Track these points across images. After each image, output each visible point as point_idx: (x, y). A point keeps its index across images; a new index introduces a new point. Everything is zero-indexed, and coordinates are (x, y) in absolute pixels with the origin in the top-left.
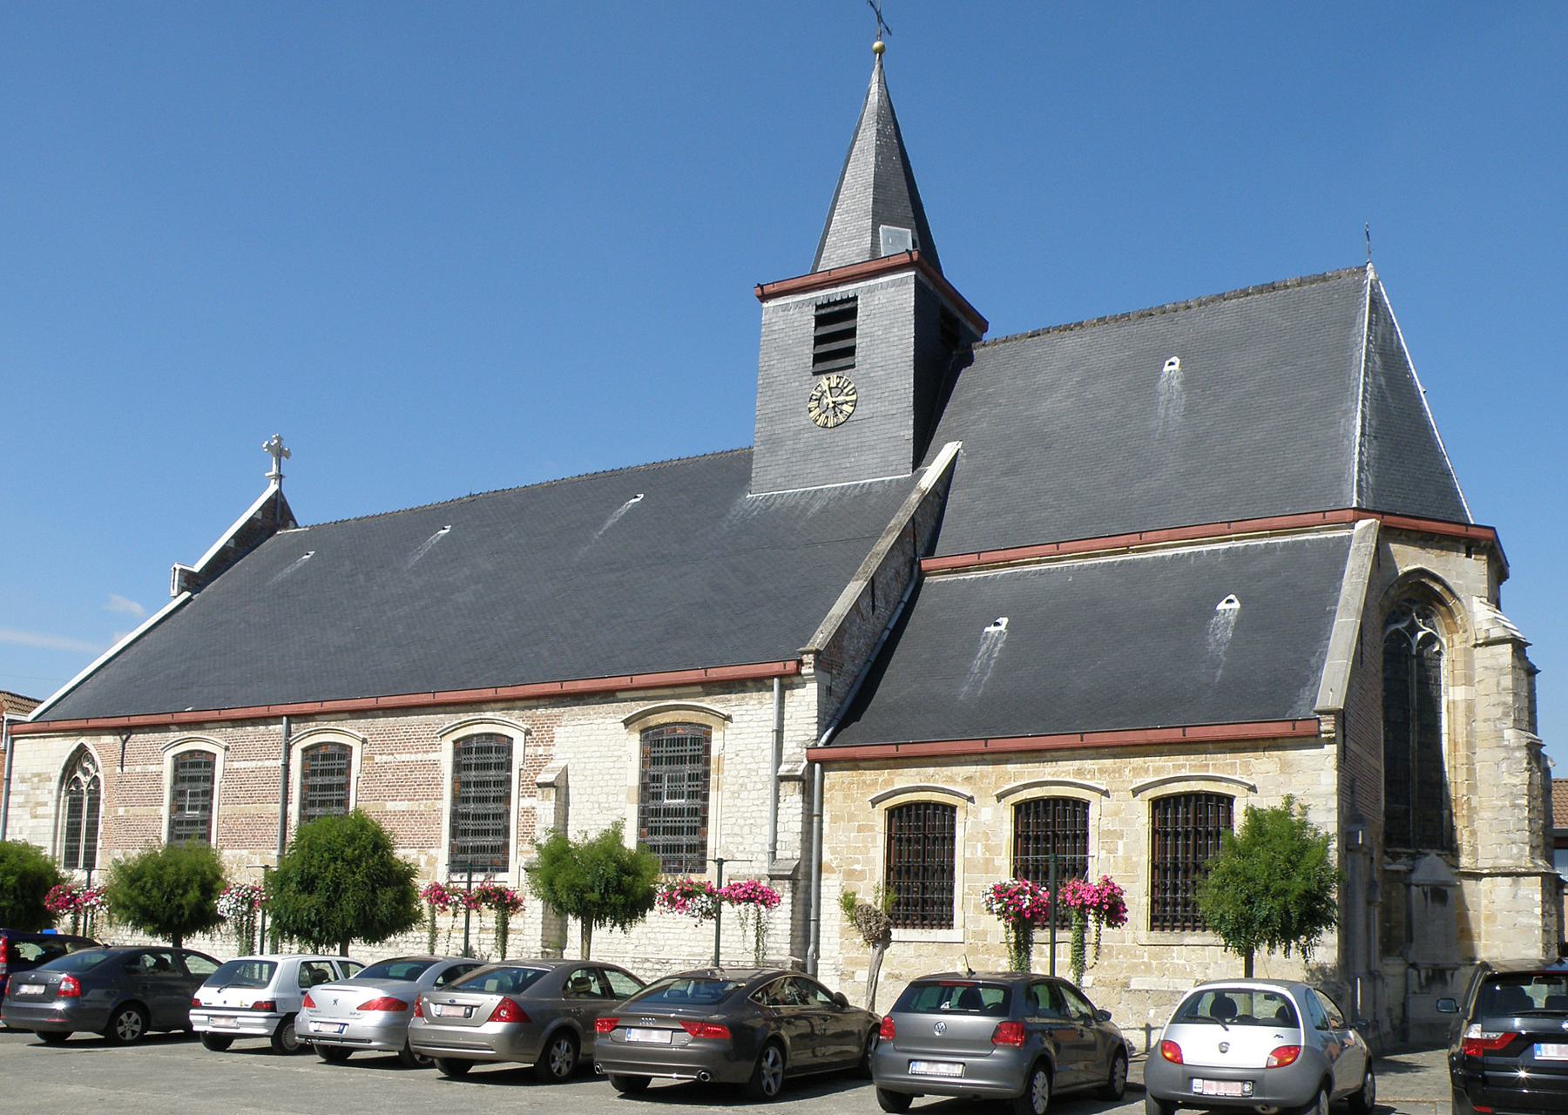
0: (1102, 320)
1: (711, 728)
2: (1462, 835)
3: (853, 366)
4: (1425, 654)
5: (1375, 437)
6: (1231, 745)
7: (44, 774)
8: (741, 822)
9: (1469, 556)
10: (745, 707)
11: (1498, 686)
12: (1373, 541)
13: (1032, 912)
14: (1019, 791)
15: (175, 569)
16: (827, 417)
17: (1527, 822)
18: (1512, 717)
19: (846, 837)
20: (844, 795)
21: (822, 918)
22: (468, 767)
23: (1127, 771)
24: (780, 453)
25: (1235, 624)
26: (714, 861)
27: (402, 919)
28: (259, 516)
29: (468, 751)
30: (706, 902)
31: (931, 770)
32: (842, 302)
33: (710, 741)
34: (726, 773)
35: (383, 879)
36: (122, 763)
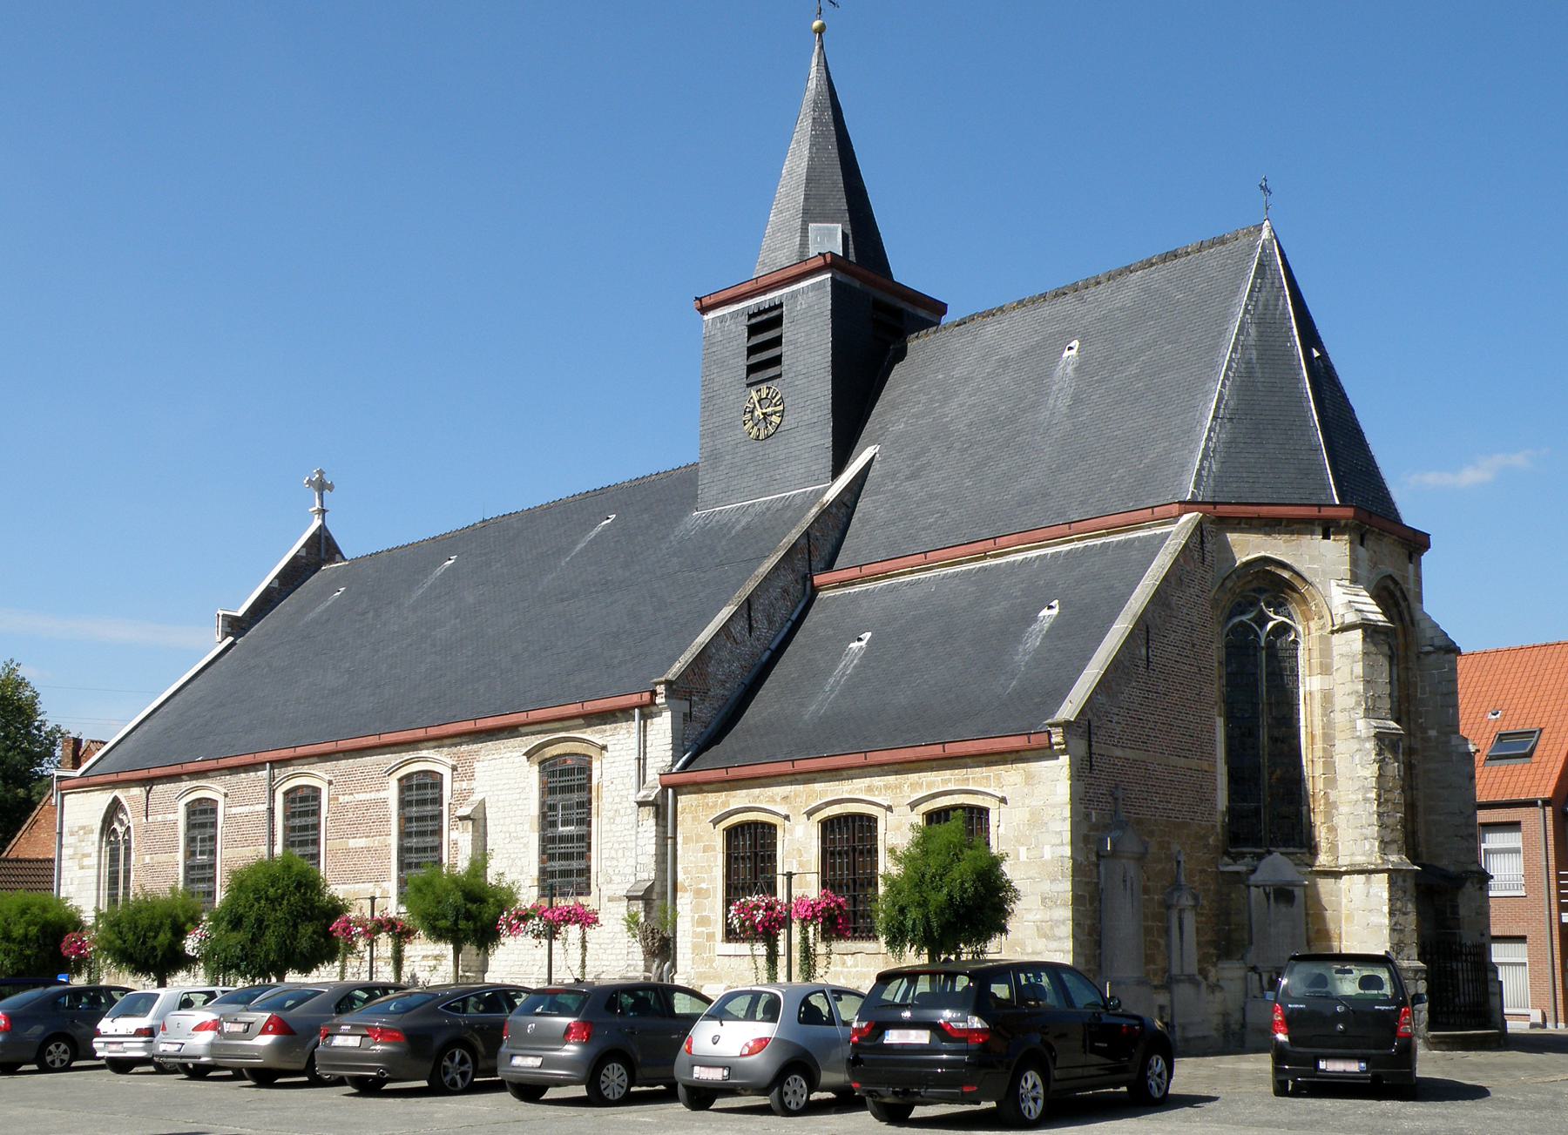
0: (1021, 303)
1: (591, 757)
2: (1320, 832)
3: (780, 376)
4: (1278, 645)
5: (1231, 419)
6: (983, 759)
7: (88, 826)
8: (616, 846)
11: (1352, 674)
12: (1184, 537)
13: (763, 926)
14: (823, 809)
15: (218, 615)
16: (759, 429)
17: (1376, 816)
18: (1364, 706)
19: (695, 857)
20: (693, 817)
21: (678, 935)
22: (410, 803)
23: (906, 786)
24: (721, 468)
25: (1047, 632)
26: (783, 875)
27: (326, 949)
28: (303, 553)
29: (410, 788)
30: (538, 925)
31: (757, 791)
32: (771, 309)
33: (591, 770)
34: (604, 800)
35: (305, 914)
36: (147, 813)
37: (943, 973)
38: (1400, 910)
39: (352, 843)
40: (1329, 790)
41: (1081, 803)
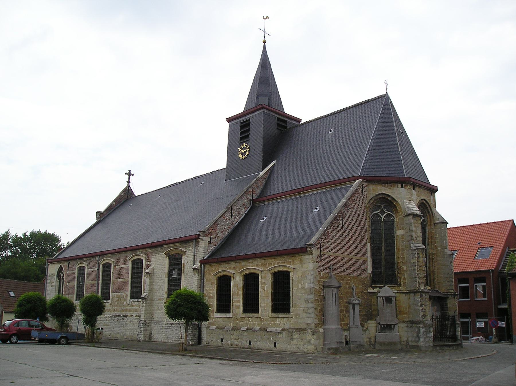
3: (249, 140)
9: (402, 187)
10: (189, 249)
23: (267, 264)
34: (185, 268)
38: (424, 305)
39: (119, 280)
40: (404, 267)
41: (317, 270)
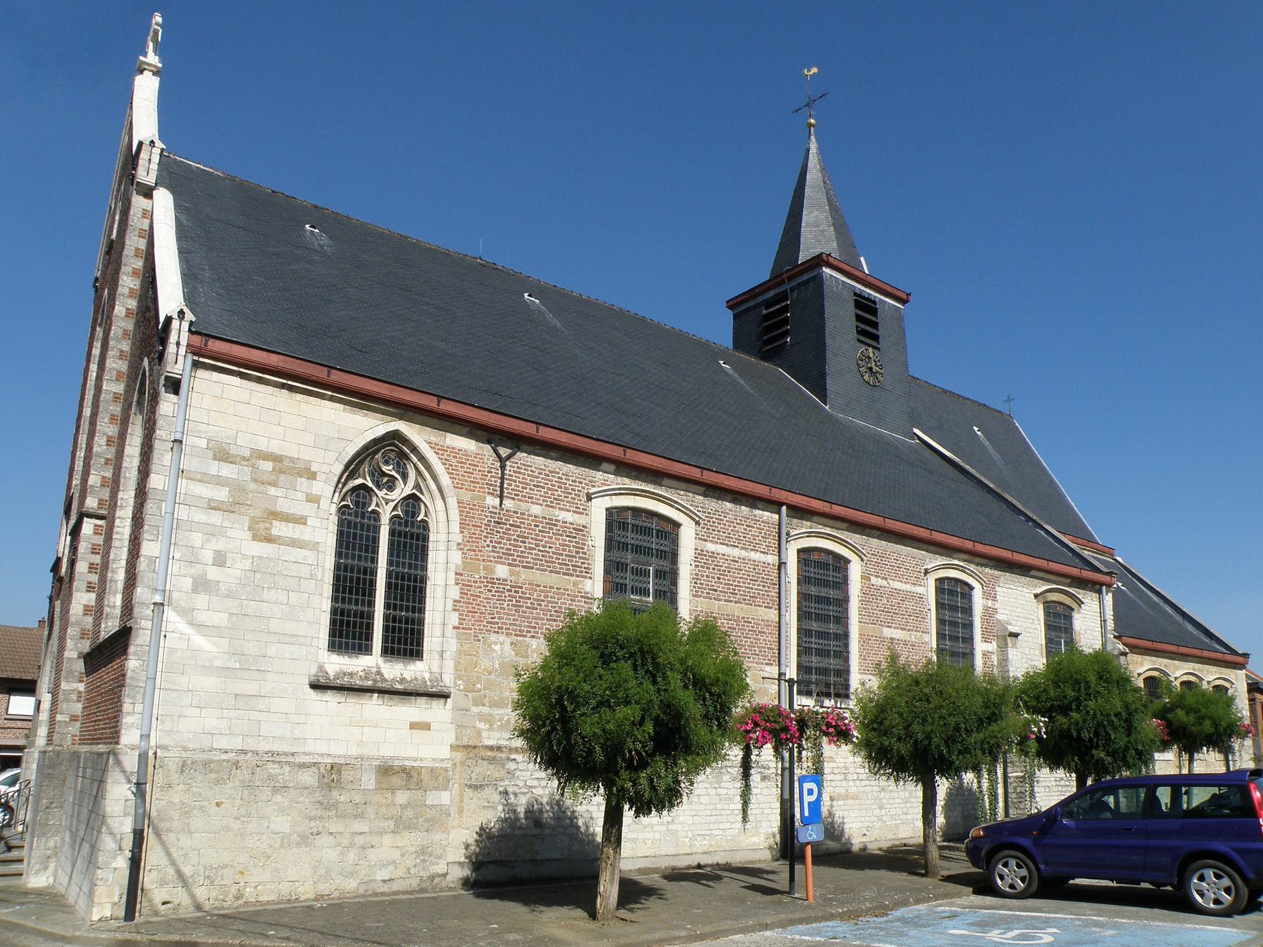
37: (1142, 786)
